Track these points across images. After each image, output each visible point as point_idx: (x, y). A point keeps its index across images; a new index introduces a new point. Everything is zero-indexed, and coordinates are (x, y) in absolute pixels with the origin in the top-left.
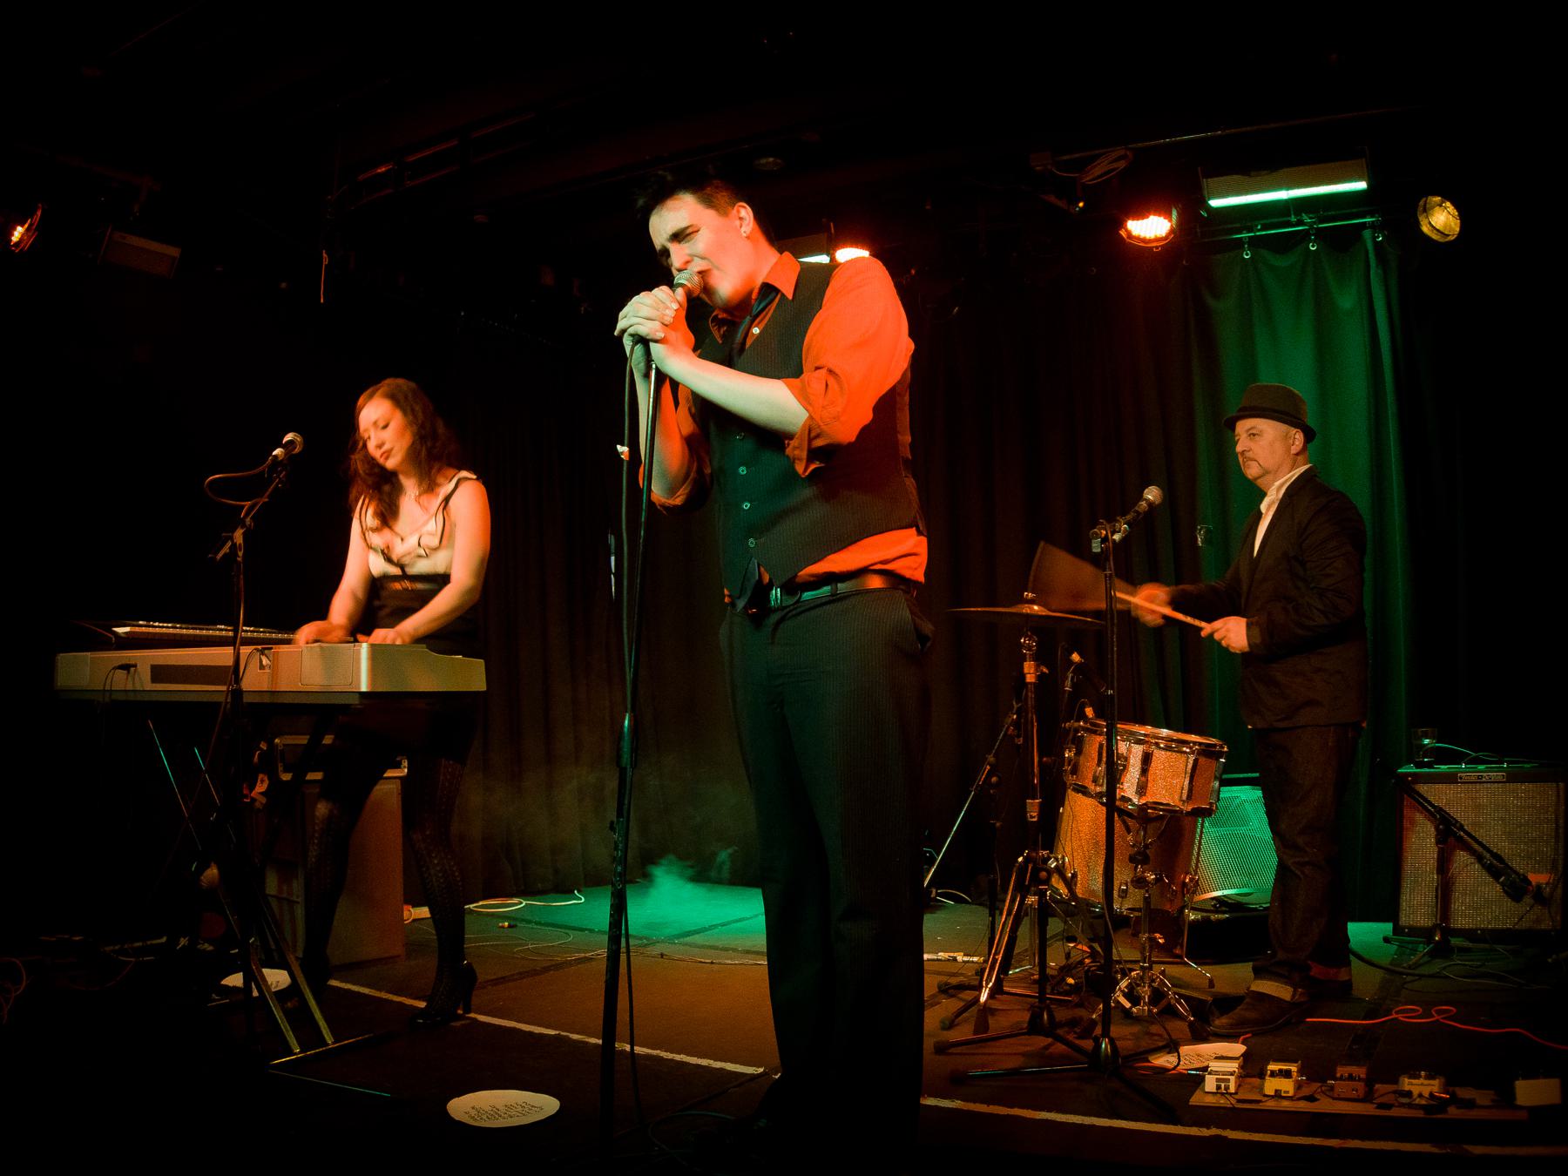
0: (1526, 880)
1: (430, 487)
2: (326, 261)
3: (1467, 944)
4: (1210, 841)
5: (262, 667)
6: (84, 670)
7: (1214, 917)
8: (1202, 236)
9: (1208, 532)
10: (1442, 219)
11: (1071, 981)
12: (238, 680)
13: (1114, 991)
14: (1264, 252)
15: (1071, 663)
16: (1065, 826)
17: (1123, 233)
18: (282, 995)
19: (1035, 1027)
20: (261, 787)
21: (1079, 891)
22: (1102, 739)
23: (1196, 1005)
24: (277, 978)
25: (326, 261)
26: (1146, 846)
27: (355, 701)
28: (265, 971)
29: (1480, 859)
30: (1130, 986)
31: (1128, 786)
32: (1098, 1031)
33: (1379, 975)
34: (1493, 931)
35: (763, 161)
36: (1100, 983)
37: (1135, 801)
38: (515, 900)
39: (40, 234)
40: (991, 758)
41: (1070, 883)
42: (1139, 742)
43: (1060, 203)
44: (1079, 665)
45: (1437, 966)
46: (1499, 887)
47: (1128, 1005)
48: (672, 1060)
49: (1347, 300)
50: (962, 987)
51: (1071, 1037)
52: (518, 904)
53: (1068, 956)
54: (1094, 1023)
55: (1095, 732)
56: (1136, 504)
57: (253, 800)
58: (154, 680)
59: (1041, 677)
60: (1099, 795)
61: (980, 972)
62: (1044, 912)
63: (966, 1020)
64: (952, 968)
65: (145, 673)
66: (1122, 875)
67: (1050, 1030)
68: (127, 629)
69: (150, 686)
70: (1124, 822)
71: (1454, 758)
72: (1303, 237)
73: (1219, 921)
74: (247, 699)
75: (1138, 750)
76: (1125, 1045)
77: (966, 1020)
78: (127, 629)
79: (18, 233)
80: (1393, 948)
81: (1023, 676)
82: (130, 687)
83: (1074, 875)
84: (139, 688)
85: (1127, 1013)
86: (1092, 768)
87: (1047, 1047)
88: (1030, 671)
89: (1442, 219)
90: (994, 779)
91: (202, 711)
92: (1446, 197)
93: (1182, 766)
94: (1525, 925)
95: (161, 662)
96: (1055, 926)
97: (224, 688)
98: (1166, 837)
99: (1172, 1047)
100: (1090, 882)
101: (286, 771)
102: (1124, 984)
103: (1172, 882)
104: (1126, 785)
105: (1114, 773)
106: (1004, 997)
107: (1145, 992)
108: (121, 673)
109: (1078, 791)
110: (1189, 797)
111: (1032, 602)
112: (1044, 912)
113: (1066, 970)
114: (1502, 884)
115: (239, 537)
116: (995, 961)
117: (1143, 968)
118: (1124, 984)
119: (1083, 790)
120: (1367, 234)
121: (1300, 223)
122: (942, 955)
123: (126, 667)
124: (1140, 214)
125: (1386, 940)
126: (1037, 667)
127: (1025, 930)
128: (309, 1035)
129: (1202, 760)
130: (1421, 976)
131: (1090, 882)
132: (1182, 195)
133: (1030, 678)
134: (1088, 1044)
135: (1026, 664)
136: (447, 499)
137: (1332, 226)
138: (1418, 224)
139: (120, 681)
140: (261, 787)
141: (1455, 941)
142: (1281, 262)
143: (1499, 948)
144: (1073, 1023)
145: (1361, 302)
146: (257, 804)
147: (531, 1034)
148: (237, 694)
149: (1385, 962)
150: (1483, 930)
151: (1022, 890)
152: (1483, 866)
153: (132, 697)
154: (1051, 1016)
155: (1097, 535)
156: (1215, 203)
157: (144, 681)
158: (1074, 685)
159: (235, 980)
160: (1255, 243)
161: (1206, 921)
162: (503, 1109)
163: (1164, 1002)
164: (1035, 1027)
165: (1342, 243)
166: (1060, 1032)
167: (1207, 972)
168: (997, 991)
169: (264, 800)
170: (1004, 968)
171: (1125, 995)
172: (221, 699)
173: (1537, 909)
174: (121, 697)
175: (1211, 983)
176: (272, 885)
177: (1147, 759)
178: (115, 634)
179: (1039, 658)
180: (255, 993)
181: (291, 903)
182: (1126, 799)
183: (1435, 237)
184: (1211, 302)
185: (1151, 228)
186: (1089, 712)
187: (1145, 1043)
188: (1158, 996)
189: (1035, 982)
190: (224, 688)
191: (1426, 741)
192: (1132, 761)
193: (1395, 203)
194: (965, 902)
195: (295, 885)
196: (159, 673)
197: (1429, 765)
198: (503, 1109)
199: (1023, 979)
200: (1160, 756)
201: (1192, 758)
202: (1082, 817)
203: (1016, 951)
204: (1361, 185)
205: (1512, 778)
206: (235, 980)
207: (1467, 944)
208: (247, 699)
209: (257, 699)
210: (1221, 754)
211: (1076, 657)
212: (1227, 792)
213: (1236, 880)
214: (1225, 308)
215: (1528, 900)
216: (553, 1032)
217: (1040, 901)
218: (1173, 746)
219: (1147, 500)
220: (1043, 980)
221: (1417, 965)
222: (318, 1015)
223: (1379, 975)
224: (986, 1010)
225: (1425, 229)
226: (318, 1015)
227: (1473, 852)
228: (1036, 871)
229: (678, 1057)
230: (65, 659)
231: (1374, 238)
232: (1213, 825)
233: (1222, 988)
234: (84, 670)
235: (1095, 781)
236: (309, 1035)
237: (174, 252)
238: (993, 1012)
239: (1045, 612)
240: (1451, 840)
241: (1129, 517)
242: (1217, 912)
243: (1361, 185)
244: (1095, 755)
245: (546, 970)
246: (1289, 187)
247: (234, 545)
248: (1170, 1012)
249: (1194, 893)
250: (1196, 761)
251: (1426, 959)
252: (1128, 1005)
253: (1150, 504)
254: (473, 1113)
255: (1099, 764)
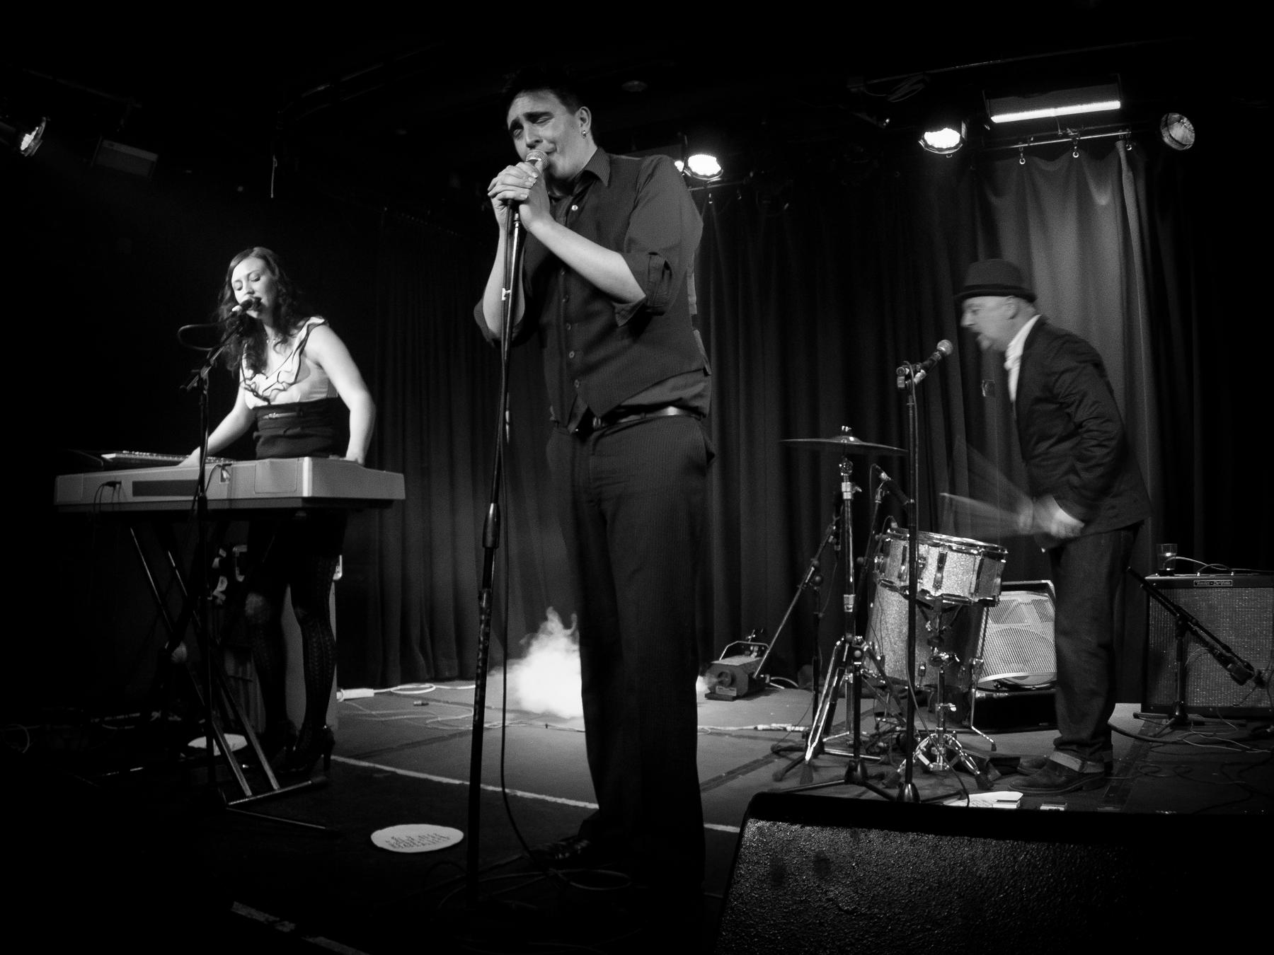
0: (1249, 666)
1: (285, 334)
2: (275, 165)
3: (1201, 718)
4: (993, 633)
5: (223, 480)
6: (78, 488)
7: (995, 695)
8: (984, 147)
9: (991, 385)
10: (1180, 132)
11: (881, 744)
12: (203, 490)
13: (914, 750)
14: (1036, 159)
15: (880, 480)
16: (875, 620)
17: (921, 143)
18: (241, 755)
19: (850, 779)
20: (222, 586)
21: (888, 670)
22: (906, 543)
23: (980, 763)
24: (236, 741)
25: (275, 165)
26: (941, 632)
27: (299, 504)
28: (227, 736)
29: (1212, 650)
30: (929, 747)
31: (926, 583)
32: (903, 780)
33: (1130, 742)
34: (1221, 709)
35: (630, 84)
36: (905, 746)
37: (933, 593)
38: (427, 685)
39: (44, 139)
40: (816, 562)
41: (880, 665)
42: (936, 545)
43: (868, 119)
44: (887, 484)
45: (1178, 736)
46: (1227, 673)
47: (926, 762)
48: (555, 803)
49: (1103, 199)
50: (791, 749)
51: (880, 786)
52: (429, 688)
53: (877, 727)
54: (899, 776)
55: (900, 538)
56: (931, 353)
57: (215, 598)
58: (135, 493)
59: (856, 495)
60: (904, 588)
61: (806, 735)
62: (858, 690)
63: (795, 774)
64: (781, 735)
65: (127, 488)
66: (921, 657)
67: (864, 781)
68: (113, 456)
69: (131, 498)
70: (923, 612)
71: (1190, 568)
72: (1067, 148)
73: (1000, 699)
74: (211, 506)
75: (934, 554)
76: (925, 793)
77: (795, 774)
78: (113, 456)
79: (27, 141)
80: (1141, 722)
81: (841, 494)
82: (115, 500)
83: (883, 658)
84: (122, 500)
85: (926, 770)
86: (897, 568)
87: (860, 795)
88: (847, 490)
89: (1180, 132)
90: (817, 578)
91: (178, 516)
92: (1184, 113)
93: (971, 565)
94: (1249, 703)
95: (141, 479)
96: (866, 705)
97: (191, 498)
98: (958, 625)
99: (963, 794)
100: (894, 663)
101: (241, 574)
102: (923, 744)
103: (961, 663)
104: (925, 581)
105: (915, 574)
106: (826, 757)
107: (939, 750)
108: (108, 489)
109: (885, 586)
110: (977, 590)
111: (848, 434)
112: (858, 690)
113: (878, 736)
114: (1229, 670)
115: (205, 372)
116: (819, 721)
117: (938, 732)
118: (923, 744)
119: (892, 588)
120: (1120, 144)
121: (1066, 136)
122: (774, 726)
123: (113, 484)
124: (936, 126)
125: (1136, 716)
126: (853, 486)
127: (842, 705)
128: (259, 782)
129: (987, 560)
130: (1165, 743)
131: (894, 663)
132: (967, 111)
133: (847, 496)
134: (894, 792)
135: (844, 484)
136: (303, 344)
137: (1093, 143)
138: (1161, 136)
139: (108, 495)
140: (222, 586)
141: (1191, 716)
142: (1049, 167)
143: (1228, 722)
144: (881, 777)
145: (1114, 205)
146: (218, 601)
147: (440, 783)
148: (203, 501)
149: (1135, 732)
150: (1214, 708)
151: (841, 667)
152: (1214, 655)
153: (117, 509)
154: (864, 769)
155: (903, 373)
156: (997, 119)
157: (127, 495)
158: (883, 499)
159: (200, 743)
160: (1028, 152)
161: (988, 700)
162: (417, 839)
163: (955, 761)
164: (850, 779)
165: (1100, 152)
166: (871, 782)
167: (991, 739)
168: (820, 750)
169: (224, 597)
170: (826, 731)
171: (924, 754)
172: (189, 507)
173: (1258, 690)
174: (109, 509)
175: (993, 745)
176: (230, 666)
177: (942, 559)
178: (104, 460)
179: (854, 480)
180: (217, 752)
181: (246, 682)
182: (925, 592)
183: (1174, 146)
184: (994, 200)
185: (944, 139)
186: (894, 525)
187: (940, 791)
188: (950, 754)
189: (850, 746)
190: (191, 498)
191: (1168, 554)
192: (930, 561)
193: (1141, 122)
194: (794, 687)
195: (249, 666)
196: (140, 488)
197: (1170, 574)
198: (417, 839)
199: (841, 744)
200: (952, 558)
201: (979, 558)
202: (891, 611)
203: (834, 723)
204: (1115, 105)
205: (1237, 584)
206: (200, 743)
207: (1201, 718)
208: (211, 506)
209: (220, 506)
210: (1001, 556)
211: (884, 475)
212: (1006, 596)
213: (1014, 665)
214: (1004, 206)
215: (1251, 683)
216: (457, 782)
217: (855, 677)
218: (965, 550)
219: (940, 351)
220: (857, 745)
221: (1159, 735)
222: (270, 774)
223: (1130, 742)
224: (811, 766)
225: (1166, 140)
226: (270, 774)
227: (1206, 644)
228: (851, 650)
229: (560, 801)
230: (62, 481)
231: (1126, 148)
232: (996, 621)
233: (1001, 751)
234: (78, 488)
235: (900, 577)
236: (259, 782)
237: (153, 157)
238: (816, 768)
239: (859, 443)
240: (1188, 634)
241: (926, 363)
242: (997, 690)
243: (1115, 105)
244: (900, 557)
245: (453, 736)
246: (1056, 105)
247: (201, 379)
248: (960, 768)
249: (980, 674)
250: (982, 562)
251: (1168, 730)
252: (926, 762)
253: (943, 354)
254: (393, 841)
255: (903, 564)
